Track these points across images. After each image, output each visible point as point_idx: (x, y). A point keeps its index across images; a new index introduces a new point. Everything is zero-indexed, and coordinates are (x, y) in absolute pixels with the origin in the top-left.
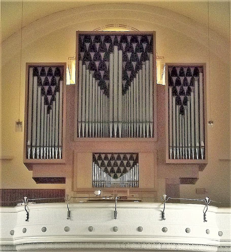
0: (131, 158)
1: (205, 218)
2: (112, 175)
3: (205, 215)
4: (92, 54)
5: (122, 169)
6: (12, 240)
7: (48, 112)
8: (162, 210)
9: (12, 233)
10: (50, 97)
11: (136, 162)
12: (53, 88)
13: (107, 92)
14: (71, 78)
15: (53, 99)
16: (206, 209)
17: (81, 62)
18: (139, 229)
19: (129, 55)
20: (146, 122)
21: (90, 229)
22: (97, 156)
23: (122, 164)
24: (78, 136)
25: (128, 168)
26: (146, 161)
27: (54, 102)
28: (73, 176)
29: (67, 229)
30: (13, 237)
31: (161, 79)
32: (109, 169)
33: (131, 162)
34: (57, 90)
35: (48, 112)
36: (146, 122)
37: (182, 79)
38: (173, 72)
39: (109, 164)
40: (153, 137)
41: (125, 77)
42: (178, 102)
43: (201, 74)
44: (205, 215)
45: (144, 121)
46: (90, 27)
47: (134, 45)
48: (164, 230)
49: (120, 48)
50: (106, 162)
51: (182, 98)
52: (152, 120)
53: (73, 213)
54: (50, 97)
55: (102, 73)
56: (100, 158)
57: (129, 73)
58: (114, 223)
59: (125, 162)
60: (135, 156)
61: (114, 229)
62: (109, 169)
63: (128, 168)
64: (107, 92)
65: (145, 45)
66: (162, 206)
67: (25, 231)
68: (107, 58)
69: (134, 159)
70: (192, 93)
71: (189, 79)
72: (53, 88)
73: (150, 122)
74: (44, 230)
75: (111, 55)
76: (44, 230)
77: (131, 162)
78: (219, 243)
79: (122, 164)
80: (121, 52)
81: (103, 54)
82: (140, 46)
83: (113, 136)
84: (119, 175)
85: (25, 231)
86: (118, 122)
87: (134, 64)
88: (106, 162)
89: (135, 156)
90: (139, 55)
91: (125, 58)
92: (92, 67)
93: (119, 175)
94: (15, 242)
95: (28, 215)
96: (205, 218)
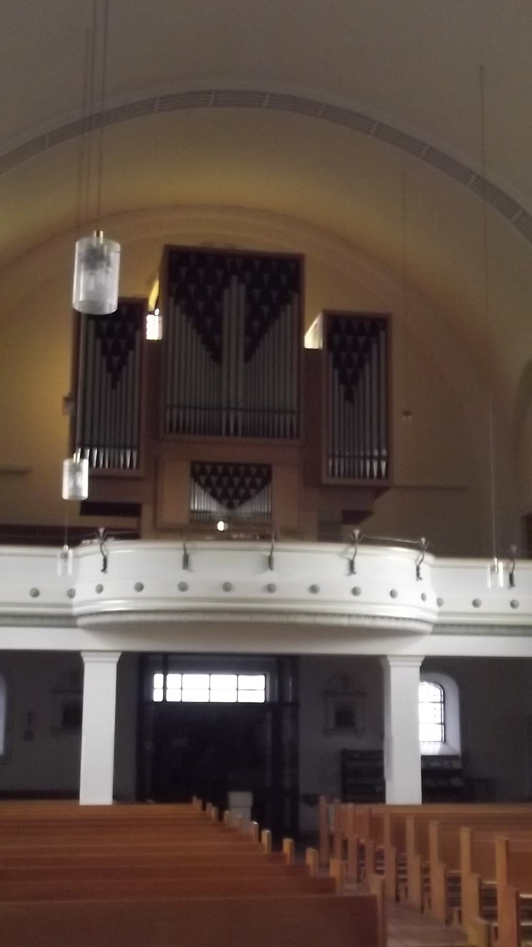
0: (259, 474)
1: (418, 574)
2: (225, 502)
3: (418, 569)
4: (192, 288)
5: (242, 492)
6: (70, 606)
7: (114, 386)
8: (351, 557)
9: (71, 594)
10: (116, 359)
11: (267, 480)
12: (123, 343)
13: (217, 357)
14: (153, 328)
15: (123, 362)
16: (420, 558)
17: (172, 301)
18: (314, 589)
19: (257, 292)
20: (228, 409)
21: (227, 587)
22: (198, 468)
23: (242, 484)
24: (165, 431)
25: (252, 492)
26: (285, 479)
27: (125, 368)
28: (155, 502)
29: (183, 587)
30: (75, 600)
31: (312, 340)
32: (219, 491)
33: (259, 481)
34: (131, 345)
35: (114, 386)
36: (228, 409)
37: (349, 339)
38: (334, 326)
39: (220, 483)
40: (298, 437)
41: (249, 331)
42: (343, 379)
43: (382, 333)
44: (418, 569)
45: (224, 405)
46: (191, 236)
47: (266, 277)
48: (355, 592)
49: (241, 280)
50: (214, 479)
51: (349, 372)
52: (295, 409)
53: (194, 559)
54: (116, 359)
55: (209, 322)
56: (203, 471)
57: (256, 324)
58: (269, 577)
59: (248, 481)
60: (265, 471)
61: (270, 588)
62: (219, 491)
63: (252, 492)
64: (217, 357)
65: (283, 278)
66: (352, 550)
67: (100, 589)
68: (218, 295)
69: (258, 478)
70: (367, 367)
71: (361, 340)
72: (123, 343)
73: (292, 412)
74: (140, 587)
75: (226, 292)
76: (140, 587)
77: (259, 481)
78: (434, 618)
79: (242, 484)
80: (243, 288)
81: (210, 289)
82: (275, 280)
83: (228, 433)
84: (236, 502)
85: (100, 589)
86: (237, 409)
87: (266, 309)
88: (214, 479)
89: (265, 471)
90: (275, 294)
91: (249, 298)
92: (189, 310)
93: (236, 502)
94: (76, 610)
95: (105, 561)
96: (418, 574)
